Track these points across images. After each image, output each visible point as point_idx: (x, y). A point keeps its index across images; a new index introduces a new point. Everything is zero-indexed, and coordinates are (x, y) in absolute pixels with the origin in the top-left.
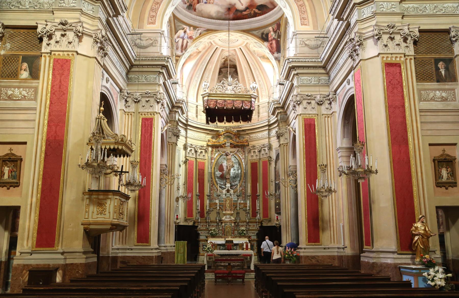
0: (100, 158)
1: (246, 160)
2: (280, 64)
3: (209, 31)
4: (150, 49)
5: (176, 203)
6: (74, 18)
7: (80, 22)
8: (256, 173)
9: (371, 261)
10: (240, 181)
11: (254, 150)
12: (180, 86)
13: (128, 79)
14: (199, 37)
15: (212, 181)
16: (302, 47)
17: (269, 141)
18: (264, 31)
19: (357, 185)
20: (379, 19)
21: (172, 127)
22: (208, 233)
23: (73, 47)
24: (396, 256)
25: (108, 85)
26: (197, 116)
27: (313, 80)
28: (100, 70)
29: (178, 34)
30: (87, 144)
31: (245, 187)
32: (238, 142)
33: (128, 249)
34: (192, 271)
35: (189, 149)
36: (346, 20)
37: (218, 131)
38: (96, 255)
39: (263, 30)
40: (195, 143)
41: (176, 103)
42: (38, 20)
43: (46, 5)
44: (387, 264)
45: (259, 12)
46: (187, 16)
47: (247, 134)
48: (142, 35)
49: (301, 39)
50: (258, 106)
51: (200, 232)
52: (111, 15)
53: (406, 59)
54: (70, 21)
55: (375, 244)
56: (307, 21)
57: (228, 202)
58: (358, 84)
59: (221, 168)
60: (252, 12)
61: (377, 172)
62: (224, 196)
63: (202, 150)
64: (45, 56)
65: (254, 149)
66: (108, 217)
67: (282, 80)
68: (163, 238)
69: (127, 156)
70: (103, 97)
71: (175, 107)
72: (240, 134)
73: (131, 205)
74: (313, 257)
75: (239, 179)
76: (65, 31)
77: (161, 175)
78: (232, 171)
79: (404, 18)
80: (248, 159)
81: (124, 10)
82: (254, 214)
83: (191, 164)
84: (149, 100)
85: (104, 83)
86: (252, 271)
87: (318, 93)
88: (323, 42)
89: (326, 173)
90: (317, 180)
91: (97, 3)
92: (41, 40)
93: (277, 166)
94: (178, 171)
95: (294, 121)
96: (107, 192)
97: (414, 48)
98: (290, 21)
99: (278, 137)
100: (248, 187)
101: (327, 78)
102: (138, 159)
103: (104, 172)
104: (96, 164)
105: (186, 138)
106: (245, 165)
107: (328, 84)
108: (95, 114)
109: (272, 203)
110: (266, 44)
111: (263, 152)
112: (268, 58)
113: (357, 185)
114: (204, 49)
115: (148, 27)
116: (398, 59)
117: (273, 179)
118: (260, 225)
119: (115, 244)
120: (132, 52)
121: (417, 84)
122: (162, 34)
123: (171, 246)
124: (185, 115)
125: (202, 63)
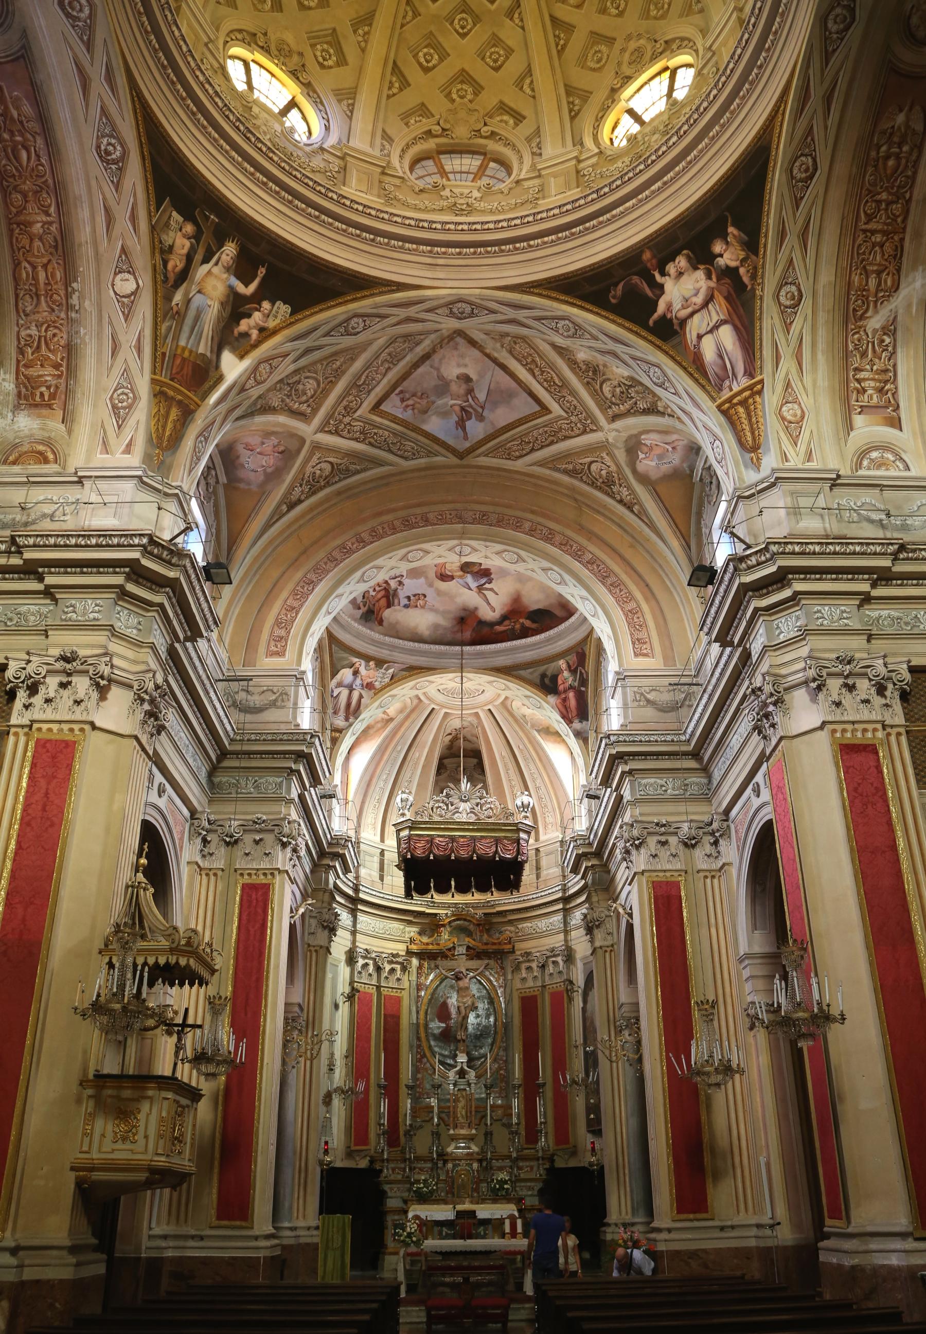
0: (130, 989)
1: (508, 990)
2: (587, 748)
3: (413, 671)
4: (271, 715)
5: (323, 1109)
6: (93, 646)
7: (105, 654)
8: (537, 1023)
9: (848, 1262)
10: (492, 1045)
11: (528, 964)
12: (342, 802)
13: (213, 787)
14: (388, 685)
15: (419, 1046)
16: (639, 706)
17: (566, 940)
18: (546, 670)
19: (797, 1055)
20: (815, 642)
21: (319, 905)
22: (409, 1190)
23: (85, 713)
24: (910, 1244)
25: (162, 803)
26: (382, 878)
27: (671, 785)
28: (143, 766)
29: (338, 676)
30: (100, 953)
31: (506, 1061)
32: (486, 944)
33: (193, 1237)
34: (362, 1306)
35: (361, 962)
36: (739, 645)
37: (436, 915)
38: (104, 1256)
40: (376, 946)
41: (329, 844)
42: (11, 650)
43: (32, 618)
44: (890, 1268)
45: (534, 626)
46: (361, 637)
47: (511, 922)
48: (251, 683)
49: (636, 689)
50: (537, 850)
51: (386, 1187)
52: (181, 637)
53: (889, 734)
54: (82, 653)
55: (853, 1213)
56: (647, 646)
57: (461, 1104)
58: (780, 796)
59: (443, 1012)
60: (518, 626)
61: (843, 1018)
62: (451, 1087)
63: (394, 966)
64: (16, 734)
65: (529, 961)
66: (142, 1149)
67: (593, 787)
68: (287, 1204)
69: (200, 985)
70: (149, 832)
71: (329, 854)
72: (491, 924)
73: (204, 1112)
74: (693, 1254)
75: (490, 1040)
76: (69, 675)
77: (285, 1031)
78: (472, 1019)
79: (873, 642)
80: (514, 989)
81: (213, 627)
82: (532, 1135)
83: (365, 1001)
84: (261, 840)
85: (153, 797)
86: (528, 1299)
87: (685, 818)
88: (689, 696)
89: (716, 1023)
90: (693, 1043)
91: (148, 611)
92: (11, 696)
93: (589, 1006)
94: (332, 1020)
95: (627, 888)
96: (144, 1080)
97: (904, 708)
98: (609, 646)
99: (589, 930)
100: (514, 1062)
101: (705, 781)
102: (228, 991)
103: (137, 1026)
104: (117, 1006)
105: (354, 933)
106: (506, 1005)
107: (707, 795)
108: (126, 875)
109: (579, 1103)
110: (552, 699)
111: (551, 968)
112: (557, 734)
113: (797, 1055)
114: (401, 711)
115: (267, 663)
116: (869, 735)
117: (580, 1040)
118: (547, 1166)
119: (158, 1223)
120: (226, 722)
121: (920, 794)
122: (299, 678)
123: (309, 1228)
124: (351, 876)
125: (396, 745)
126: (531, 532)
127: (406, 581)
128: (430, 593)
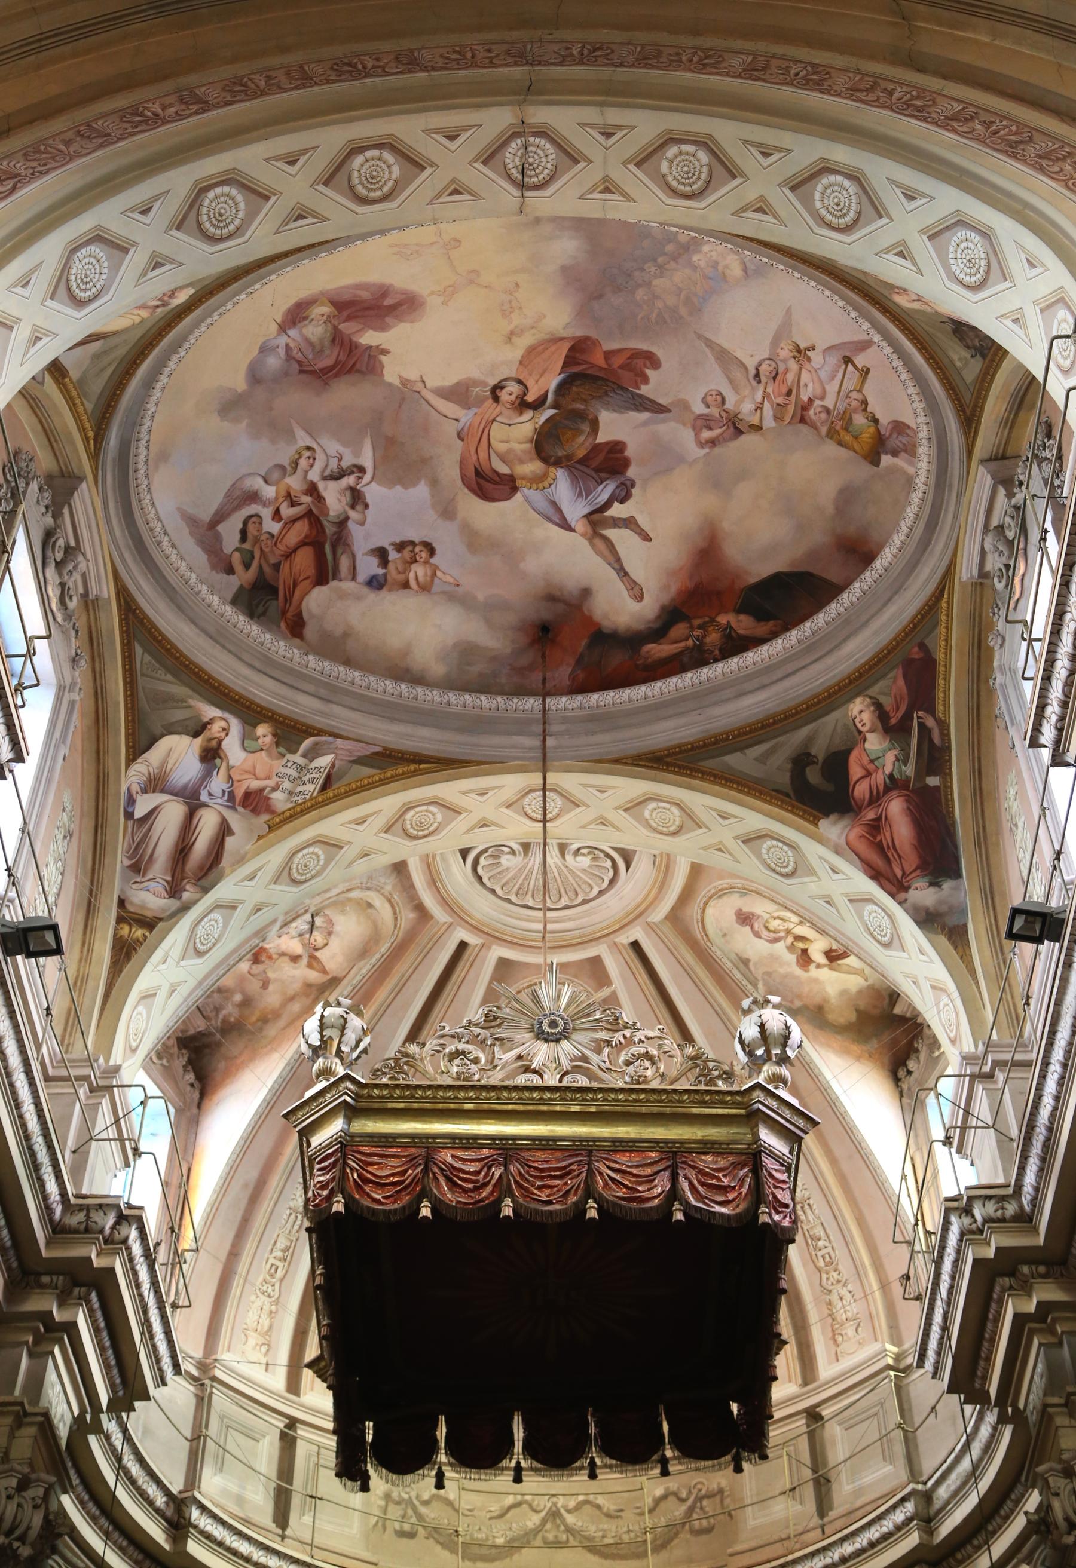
3: (394, 765)
18: (810, 740)
29: (155, 756)
39: (805, 732)
41: (58, 1231)
50: (813, 1415)
110: (833, 829)
114: (364, 952)
126: (752, 72)
127: (373, 492)
128: (446, 538)
